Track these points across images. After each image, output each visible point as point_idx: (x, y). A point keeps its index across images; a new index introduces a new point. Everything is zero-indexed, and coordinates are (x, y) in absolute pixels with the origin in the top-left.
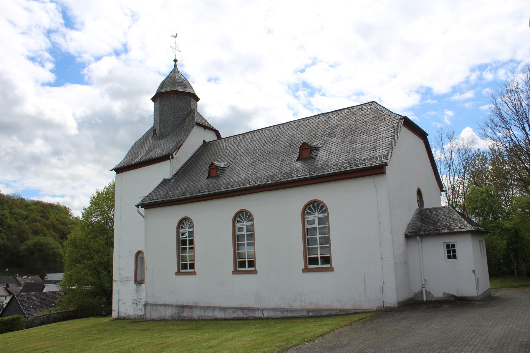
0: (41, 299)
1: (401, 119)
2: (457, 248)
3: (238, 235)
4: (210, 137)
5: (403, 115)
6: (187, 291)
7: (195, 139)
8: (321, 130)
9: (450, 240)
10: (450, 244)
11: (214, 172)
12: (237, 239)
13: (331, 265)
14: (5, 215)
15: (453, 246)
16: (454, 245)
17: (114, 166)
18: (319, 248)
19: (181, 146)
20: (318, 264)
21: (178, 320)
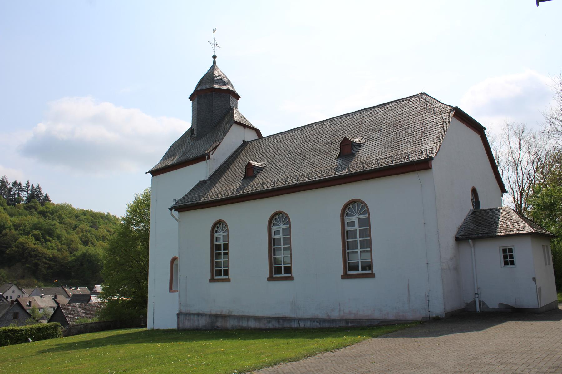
0: (86, 311)
1: (451, 111)
2: (516, 254)
3: (274, 239)
4: (250, 136)
5: (454, 106)
6: (220, 299)
7: (232, 140)
8: (365, 125)
9: (507, 244)
10: (507, 248)
11: (251, 172)
12: (272, 243)
13: (372, 271)
14: (55, 225)
15: (511, 250)
16: (512, 249)
17: (150, 169)
18: (359, 252)
19: (218, 146)
20: (281, 273)
21: (211, 330)
